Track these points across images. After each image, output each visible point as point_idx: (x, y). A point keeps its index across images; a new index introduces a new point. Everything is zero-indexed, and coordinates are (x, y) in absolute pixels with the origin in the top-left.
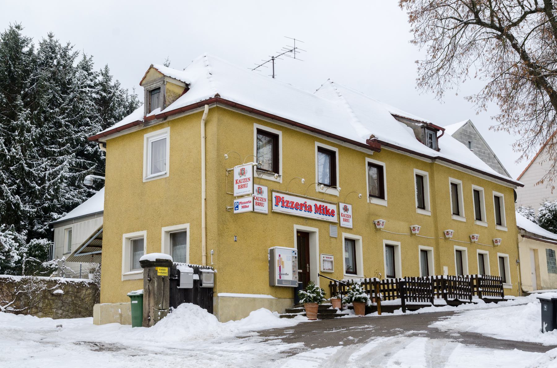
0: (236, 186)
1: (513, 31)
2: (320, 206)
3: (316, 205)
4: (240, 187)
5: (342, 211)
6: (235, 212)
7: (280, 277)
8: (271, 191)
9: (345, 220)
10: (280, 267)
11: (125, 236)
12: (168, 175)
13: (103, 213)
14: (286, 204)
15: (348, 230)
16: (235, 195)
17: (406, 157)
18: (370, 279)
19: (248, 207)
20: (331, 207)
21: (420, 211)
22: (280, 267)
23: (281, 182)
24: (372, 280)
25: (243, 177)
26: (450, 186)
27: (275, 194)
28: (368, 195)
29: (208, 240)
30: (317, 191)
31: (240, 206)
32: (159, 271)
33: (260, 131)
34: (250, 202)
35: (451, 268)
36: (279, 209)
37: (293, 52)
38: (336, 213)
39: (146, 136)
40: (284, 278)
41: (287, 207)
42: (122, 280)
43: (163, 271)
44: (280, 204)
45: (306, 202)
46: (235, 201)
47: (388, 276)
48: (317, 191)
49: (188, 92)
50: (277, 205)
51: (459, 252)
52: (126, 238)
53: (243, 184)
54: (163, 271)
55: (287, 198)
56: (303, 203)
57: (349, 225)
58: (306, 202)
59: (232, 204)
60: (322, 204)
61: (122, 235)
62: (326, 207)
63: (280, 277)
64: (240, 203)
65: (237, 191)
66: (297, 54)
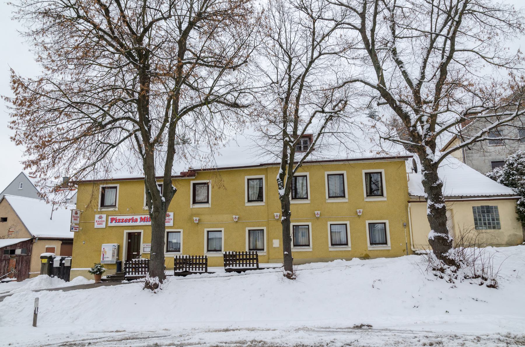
7: (103, 259)
10: (103, 254)
13: (72, 244)
14: (119, 221)
17: (240, 170)
18: (229, 253)
22: (103, 254)
24: (231, 254)
31: (74, 228)
36: (114, 224)
40: (105, 259)
41: (119, 222)
44: (114, 221)
47: (250, 249)
49: (505, 187)
55: (118, 218)
63: (103, 259)
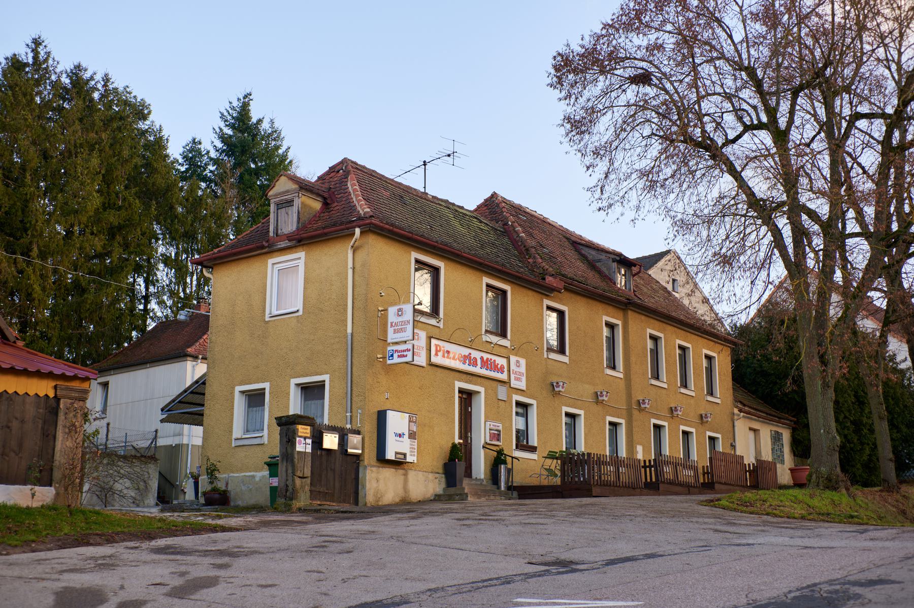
0: (390, 331)
1: (728, 150)
2: (487, 359)
3: (482, 358)
4: (395, 332)
5: (513, 367)
6: (389, 362)
8: (430, 338)
9: (517, 379)
11: (294, 381)
12: (300, 313)
15: (520, 392)
16: (389, 341)
19: (406, 356)
20: (501, 362)
21: (610, 372)
23: (442, 326)
25: (400, 319)
26: (608, 426)
27: (434, 342)
28: (545, 349)
29: (354, 395)
30: (484, 340)
31: (396, 355)
32: (300, 430)
33: (488, 286)
34: (408, 350)
35: (646, 450)
37: (452, 157)
38: (506, 370)
39: (271, 261)
42: (233, 445)
43: (305, 431)
45: (470, 354)
46: (389, 348)
48: (484, 340)
50: (436, 355)
51: (658, 427)
52: (241, 392)
53: (400, 327)
54: (305, 431)
56: (467, 354)
57: (522, 385)
58: (470, 354)
59: (384, 353)
60: (490, 356)
61: (233, 388)
62: (495, 361)
64: (396, 351)
65: (391, 336)
66: (457, 161)
